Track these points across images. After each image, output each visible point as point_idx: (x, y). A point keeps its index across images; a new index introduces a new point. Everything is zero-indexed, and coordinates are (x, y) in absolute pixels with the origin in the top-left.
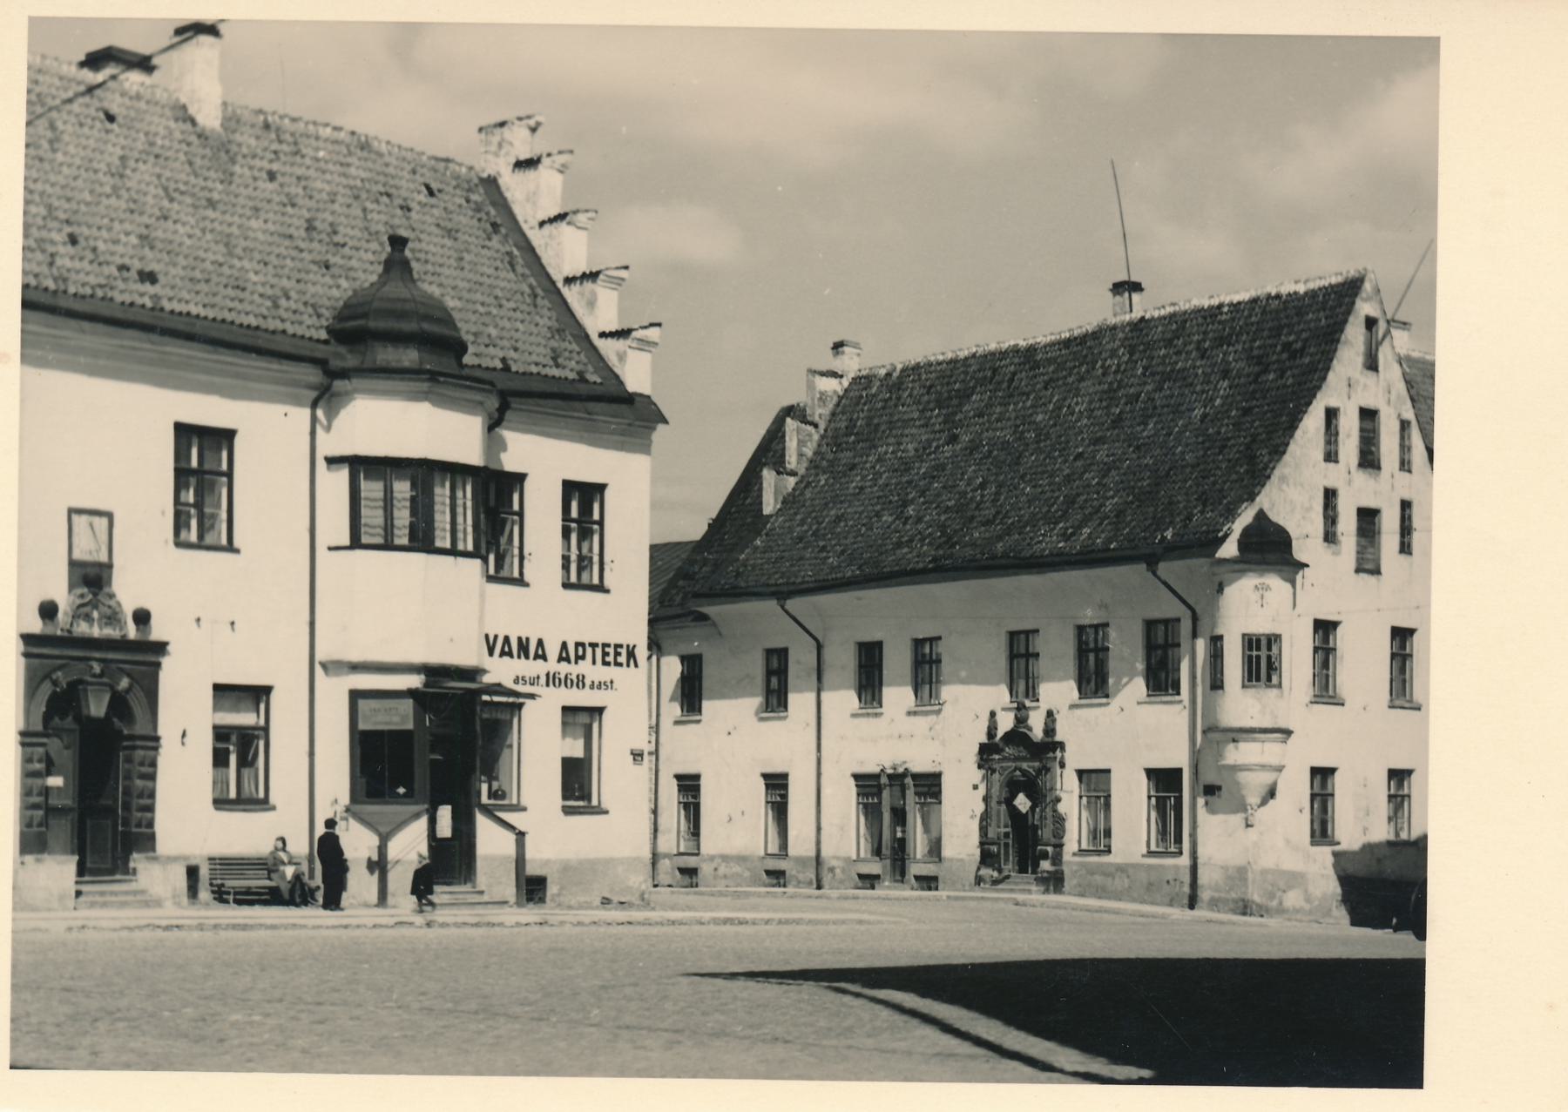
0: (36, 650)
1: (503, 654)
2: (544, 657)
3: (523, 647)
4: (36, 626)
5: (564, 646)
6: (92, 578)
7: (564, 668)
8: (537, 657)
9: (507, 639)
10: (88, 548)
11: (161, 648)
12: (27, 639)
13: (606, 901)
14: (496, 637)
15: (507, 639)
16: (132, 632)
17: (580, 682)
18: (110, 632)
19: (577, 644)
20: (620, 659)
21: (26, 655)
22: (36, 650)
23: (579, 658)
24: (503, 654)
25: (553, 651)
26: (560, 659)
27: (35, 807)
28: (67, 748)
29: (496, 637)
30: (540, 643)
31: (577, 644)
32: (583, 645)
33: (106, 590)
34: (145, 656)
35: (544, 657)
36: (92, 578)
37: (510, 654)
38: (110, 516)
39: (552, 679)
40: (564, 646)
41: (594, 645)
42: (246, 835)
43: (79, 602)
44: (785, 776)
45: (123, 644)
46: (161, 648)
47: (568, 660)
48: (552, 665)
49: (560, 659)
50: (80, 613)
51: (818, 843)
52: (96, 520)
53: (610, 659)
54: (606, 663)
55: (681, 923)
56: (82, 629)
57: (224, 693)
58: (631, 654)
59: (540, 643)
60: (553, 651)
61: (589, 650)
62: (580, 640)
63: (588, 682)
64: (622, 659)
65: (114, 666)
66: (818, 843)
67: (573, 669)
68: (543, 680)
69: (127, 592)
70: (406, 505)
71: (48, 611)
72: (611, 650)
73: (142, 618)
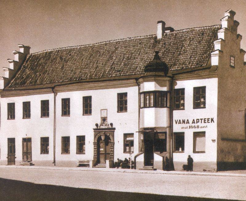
0: (95, 131)
1: (179, 123)
2: (189, 123)
3: (184, 122)
4: (95, 127)
5: (194, 120)
6: (104, 119)
7: (193, 125)
8: (187, 123)
9: (180, 121)
10: (104, 115)
11: (114, 129)
12: (94, 129)
13: (205, 170)
14: (177, 120)
15: (180, 121)
16: (110, 126)
17: (198, 127)
18: (106, 127)
19: (197, 120)
20: (209, 121)
21: (94, 132)
22: (95, 131)
23: (197, 122)
24: (179, 123)
25: (191, 122)
26: (193, 123)
27: (95, 153)
28: (104, 144)
29: (177, 120)
30: (188, 120)
31: (197, 120)
32: (199, 120)
33: (106, 121)
34: (112, 130)
35: (189, 123)
36: (104, 119)
37: (181, 123)
38: (101, 110)
39: (190, 127)
40: (194, 120)
41: (201, 119)
42: (81, 157)
43: (101, 123)
44: (14, 139)
45: (108, 129)
46: (114, 129)
47: (195, 123)
48: (191, 124)
49: (193, 123)
50: (101, 125)
51: (54, 159)
52: (105, 110)
53: (207, 121)
54: (204, 122)
55: (233, 176)
56: (102, 127)
57: (126, 135)
58: (212, 120)
59: (188, 120)
60: (191, 122)
61: (200, 121)
62: (198, 118)
63: (200, 127)
64: (210, 121)
65: (107, 132)
66: (54, 159)
67: (196, 125)
68: (188, 127)
69: (109, 121)
70: (158, 100)
71: (97, 125)
72: (207, 120)
73: (112, 124)
